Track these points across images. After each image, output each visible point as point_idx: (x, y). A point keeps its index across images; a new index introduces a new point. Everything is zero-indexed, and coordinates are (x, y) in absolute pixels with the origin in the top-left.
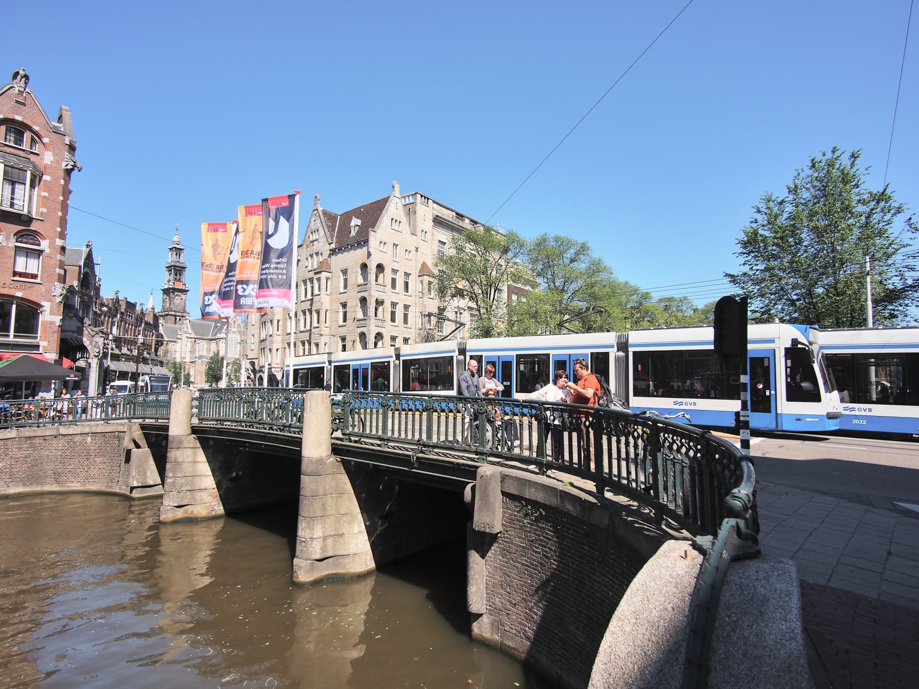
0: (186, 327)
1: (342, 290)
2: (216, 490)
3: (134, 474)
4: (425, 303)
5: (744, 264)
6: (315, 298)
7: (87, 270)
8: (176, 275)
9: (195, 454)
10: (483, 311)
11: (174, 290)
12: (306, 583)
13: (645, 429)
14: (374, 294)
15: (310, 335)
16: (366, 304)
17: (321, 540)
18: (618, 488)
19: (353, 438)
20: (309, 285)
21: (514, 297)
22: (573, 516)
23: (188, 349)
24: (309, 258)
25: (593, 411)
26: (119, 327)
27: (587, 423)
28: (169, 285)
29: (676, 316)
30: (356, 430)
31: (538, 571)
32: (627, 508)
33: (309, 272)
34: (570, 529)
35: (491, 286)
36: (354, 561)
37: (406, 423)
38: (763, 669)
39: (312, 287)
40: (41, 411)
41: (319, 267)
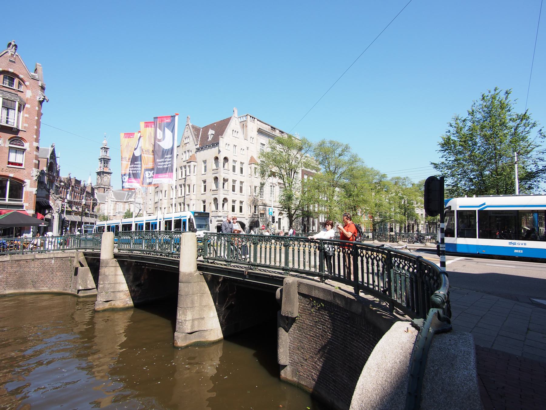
1: (203, 173)
2: (128, 291)
4: (253, 180)
5: (442, 157)
6: (187, 177)
7: (52, 161)
8: (105, 164)
9: (116, 270)
13: (383, 255)
14: (221, 176)
15: (184, 200)
16: (217, 181)
17: (191, 321)
18: (367, 291)
19: (210, 261)
21: (306, 177)
22: (341, 307)
28: (101, 170)
29: (402, 188)
30: (212, 256)
31: (320, 340)
34: (339, 315)
35: (292, 170)
38: (454, 398)
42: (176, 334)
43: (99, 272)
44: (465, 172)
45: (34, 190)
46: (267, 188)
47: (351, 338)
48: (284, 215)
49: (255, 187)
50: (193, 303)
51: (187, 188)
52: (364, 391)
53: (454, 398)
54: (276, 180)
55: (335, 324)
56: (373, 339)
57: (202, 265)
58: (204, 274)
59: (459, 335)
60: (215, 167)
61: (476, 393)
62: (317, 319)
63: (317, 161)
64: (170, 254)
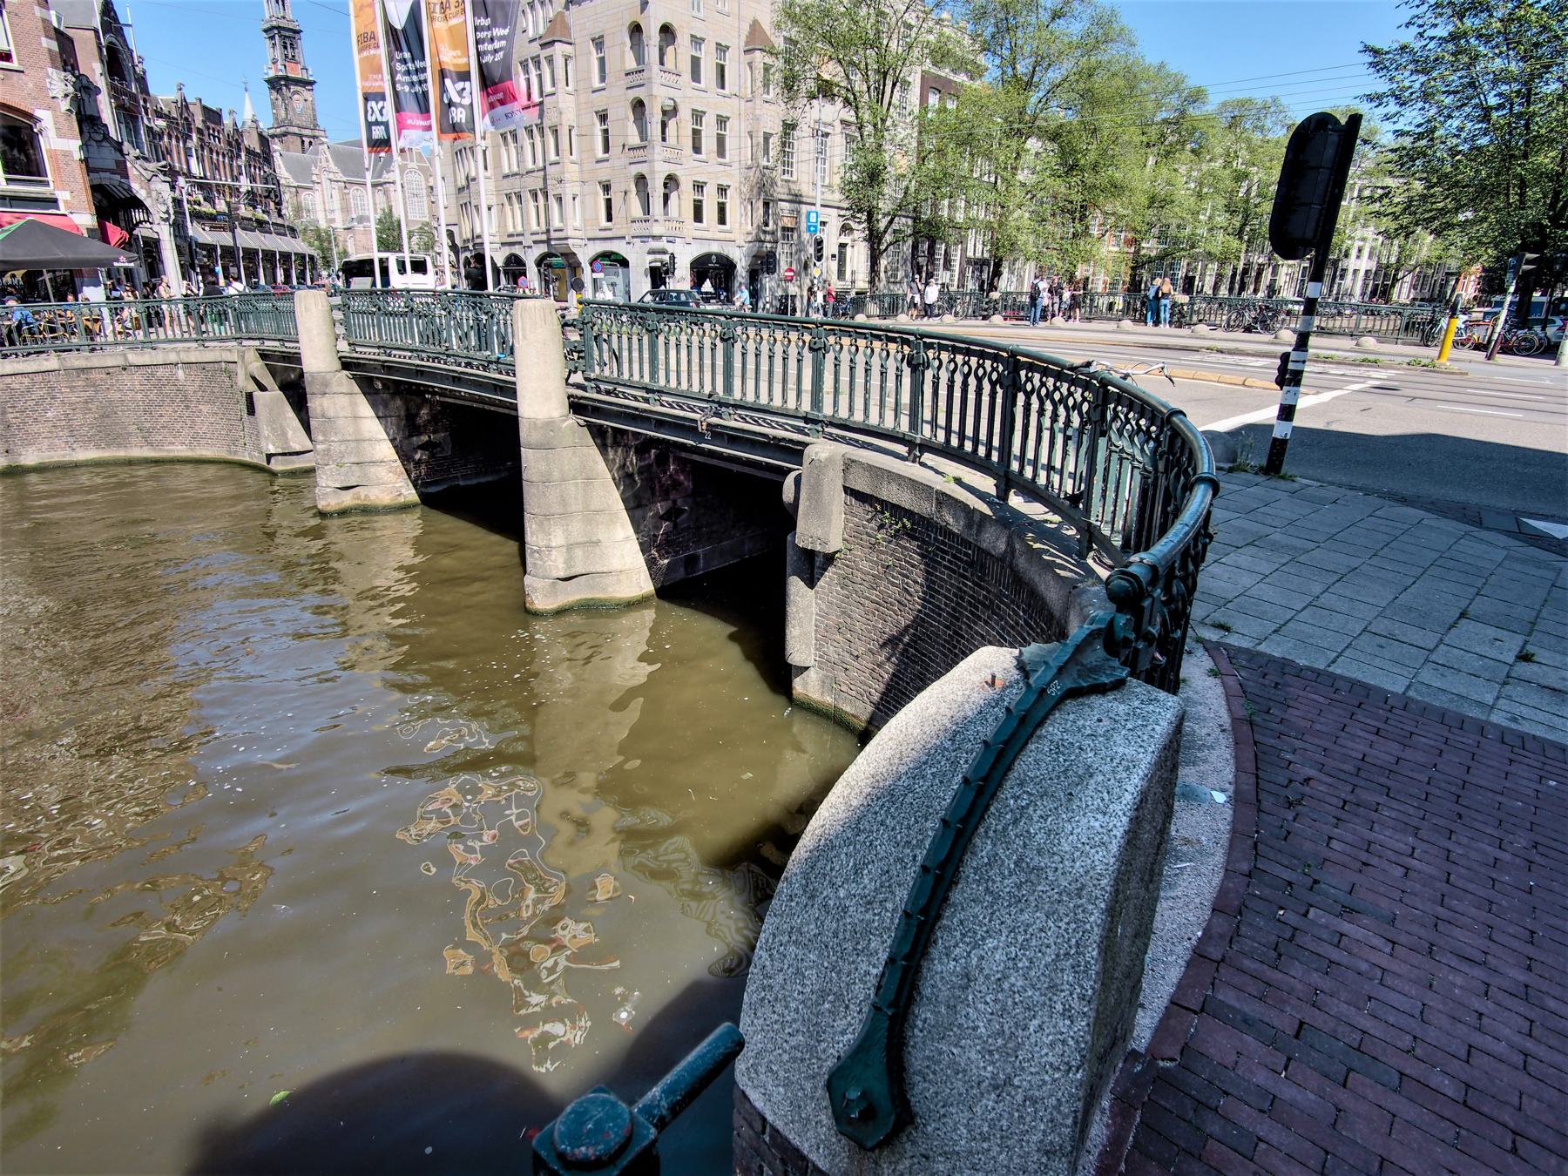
0: (325, 164)
1: (597, 84)
2: (399, 463)
3: (266, 433)
4: (757, 112)
5: (1407, 25)
6: (547, 100)
7: (110, 37)
8: (285, 48)
9: (354, 404)
10: (869, 129)
11: (289, 81)
12: (547, 612)
13: (1086, 394)
14: (658, 96)
15: (545, 179)
16: (643, 114)
17: (564, 550)
18: (1032, 492)
19: (603, 387)
20: (533, 73)
21: (933, 100)
22: (954, 534)
23: (337, 205)
24: (528, 10)
25: (1005, 354)
26: (200, 160)
27: (994, 376)
28: (277, 70)
29: (1248, 141)
30: (607, 373)
31: (894, 612)
32: (1038, 528)
33: (530, 41)
34: (946, 553)
35: (886, 75)
36: (619, 581)
37: (689, 362)
38: (1040, 888)
39: (540, 76)
40: (89, 324)
41: (550, 31)
42: (528, 580)
43: (307, 408)
44: (1472, 85)
45: (73, 145)
46: (804, 144)
47: (971, 612)
48: (856, 234)
49: (767, 137)
50: (564, 502)
51: (548, 133)
52: (823, 841)
53: (1040, 888)
54: (831, 112)
55: (936, 576)
56: (1025, 621)
57: (582, 398)
58: (589, 426)
59: (1136, 703)
60: (631, 64)
61: (1104, 882)
62: (890, 561)
63: (974, 37)
64: (490, 362)
